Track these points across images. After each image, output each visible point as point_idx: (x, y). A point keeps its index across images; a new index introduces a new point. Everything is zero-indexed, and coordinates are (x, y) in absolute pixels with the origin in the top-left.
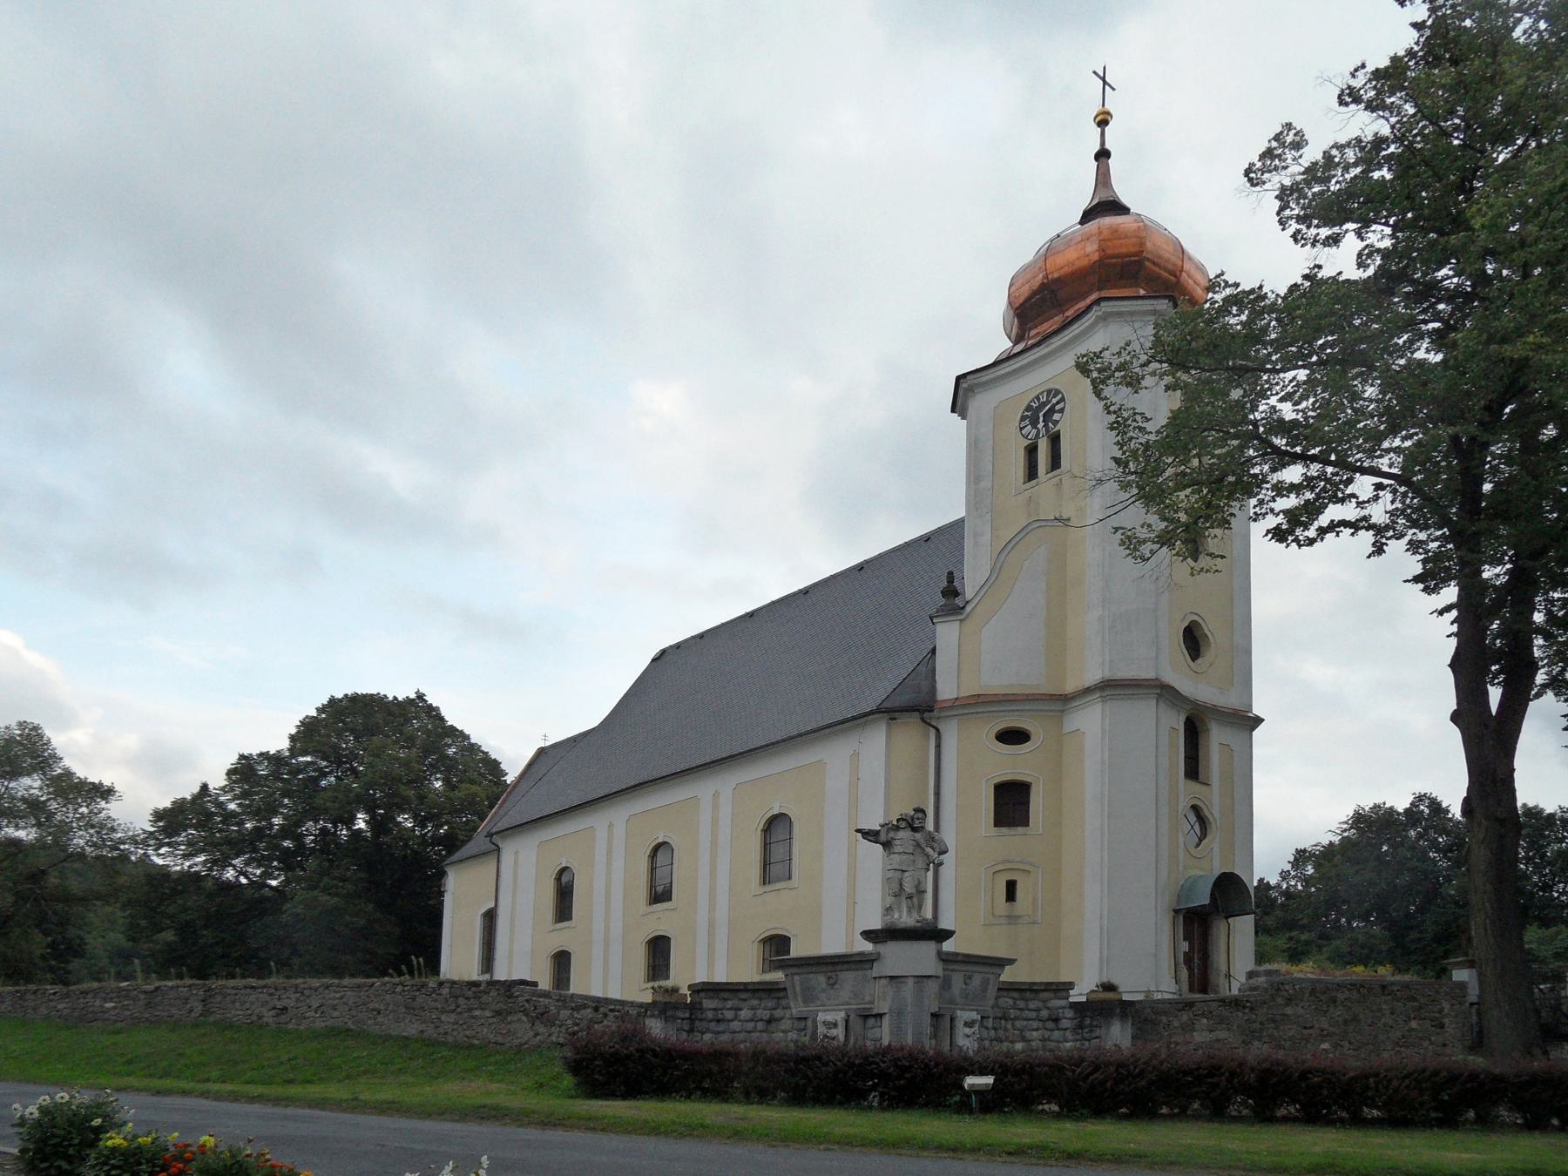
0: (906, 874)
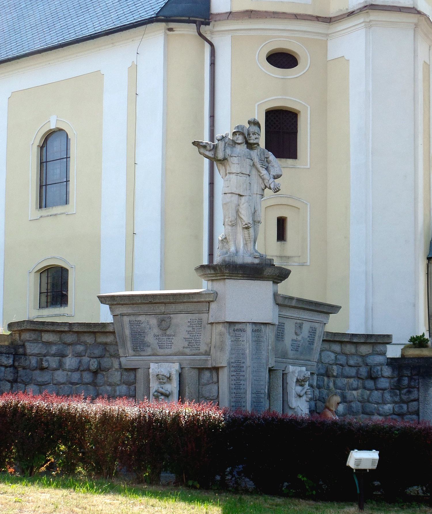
0: (243, 198)
